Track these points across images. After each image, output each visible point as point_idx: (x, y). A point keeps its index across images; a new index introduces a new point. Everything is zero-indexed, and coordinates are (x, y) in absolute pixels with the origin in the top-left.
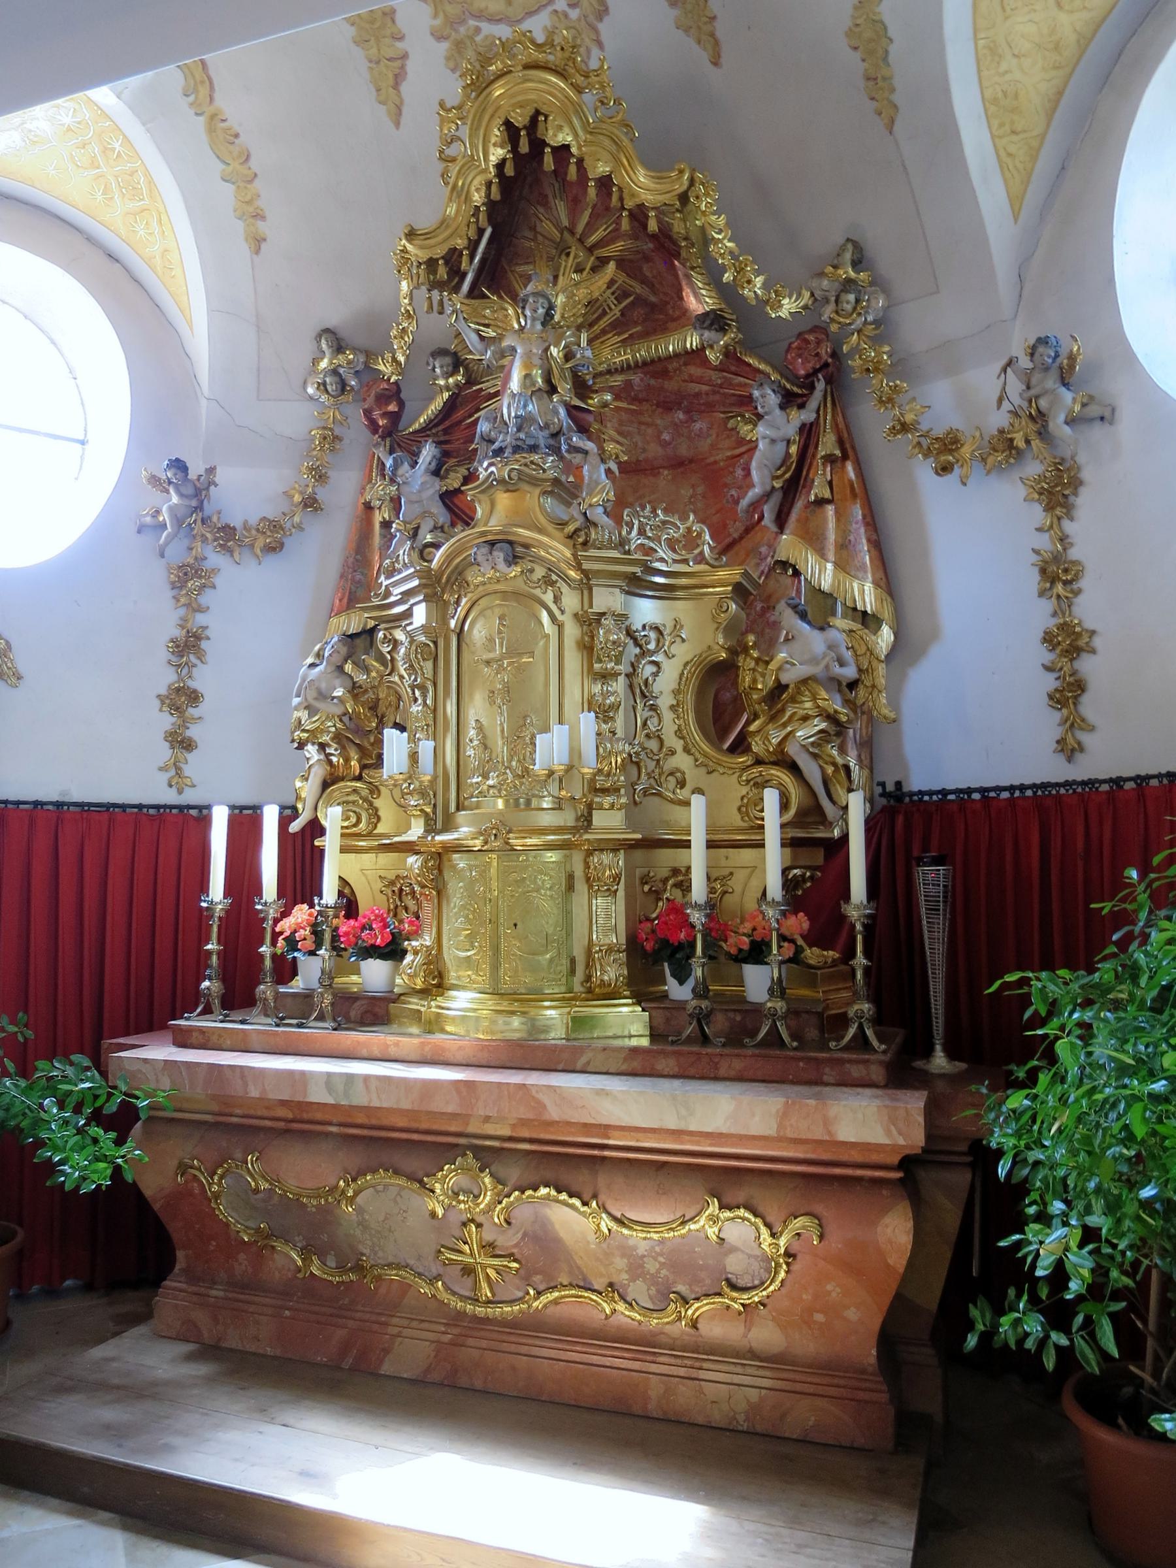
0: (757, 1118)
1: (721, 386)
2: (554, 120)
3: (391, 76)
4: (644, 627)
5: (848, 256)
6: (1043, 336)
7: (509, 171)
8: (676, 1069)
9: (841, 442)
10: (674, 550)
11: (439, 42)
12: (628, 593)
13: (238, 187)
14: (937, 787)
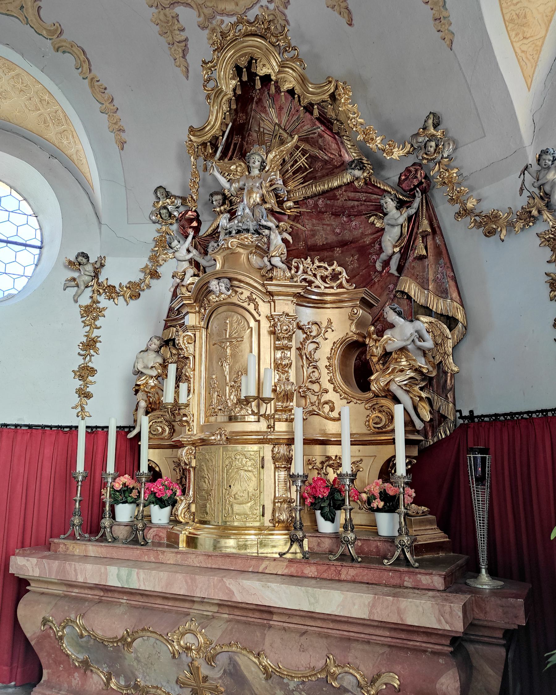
0: (356, 607)
1: (365, 201)
2: (260, 62)
3: (180, 51)
4: (309, 323)
5: (430, 121)
6: (545, 149)
7: (239, 92)
8: (316, 574)
9: (431, 225)
10: (325, 281)
11: (203, 30)
12: (297, 304)
13: (109, 115)
14: (492, 412)
